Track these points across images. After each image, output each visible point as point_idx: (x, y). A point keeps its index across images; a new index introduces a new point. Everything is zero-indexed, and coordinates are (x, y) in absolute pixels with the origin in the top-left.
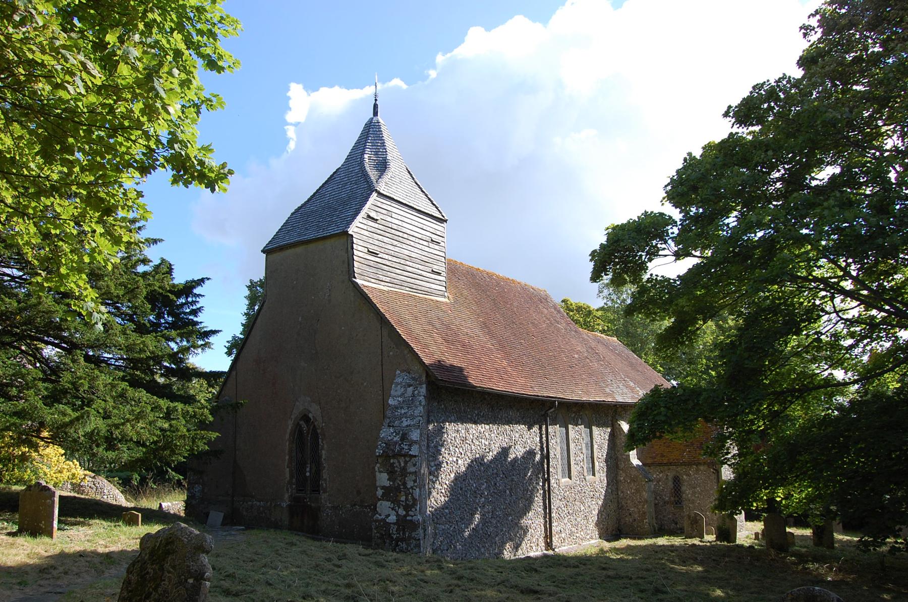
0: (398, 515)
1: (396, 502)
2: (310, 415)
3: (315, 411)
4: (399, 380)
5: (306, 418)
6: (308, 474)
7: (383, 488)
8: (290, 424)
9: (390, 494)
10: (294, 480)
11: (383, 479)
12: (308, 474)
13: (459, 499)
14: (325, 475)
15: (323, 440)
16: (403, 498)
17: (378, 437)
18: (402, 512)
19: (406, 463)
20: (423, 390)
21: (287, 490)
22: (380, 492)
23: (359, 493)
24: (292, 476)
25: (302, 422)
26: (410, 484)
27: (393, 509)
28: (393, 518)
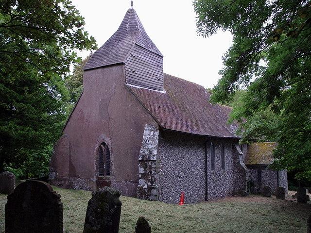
0: (148, 185)
1: (147, 180)
2: (106, 142)
3: (107, 141)
4: (147, 128)
5: (104, 144)
6: (105, 168)
7: (141, 174)
8: (97, 147)
9: (144, 176)
10: (98, 170)
11: (142, 170)
12: (105, 168)
13: (171, 179)
14: (113, 168)
15: (112, 153)
16: (150, 178)
17: (139, 153)
18: (149, 184)
19: (151, 163)
20: (157, 133)
21: (95, 174)
22: (140, 176)
23: (128, 176)
24: (97, 169)
25: (102, 145)
26: (153, 172)
27: (146, 183)
28: (146, 186)
